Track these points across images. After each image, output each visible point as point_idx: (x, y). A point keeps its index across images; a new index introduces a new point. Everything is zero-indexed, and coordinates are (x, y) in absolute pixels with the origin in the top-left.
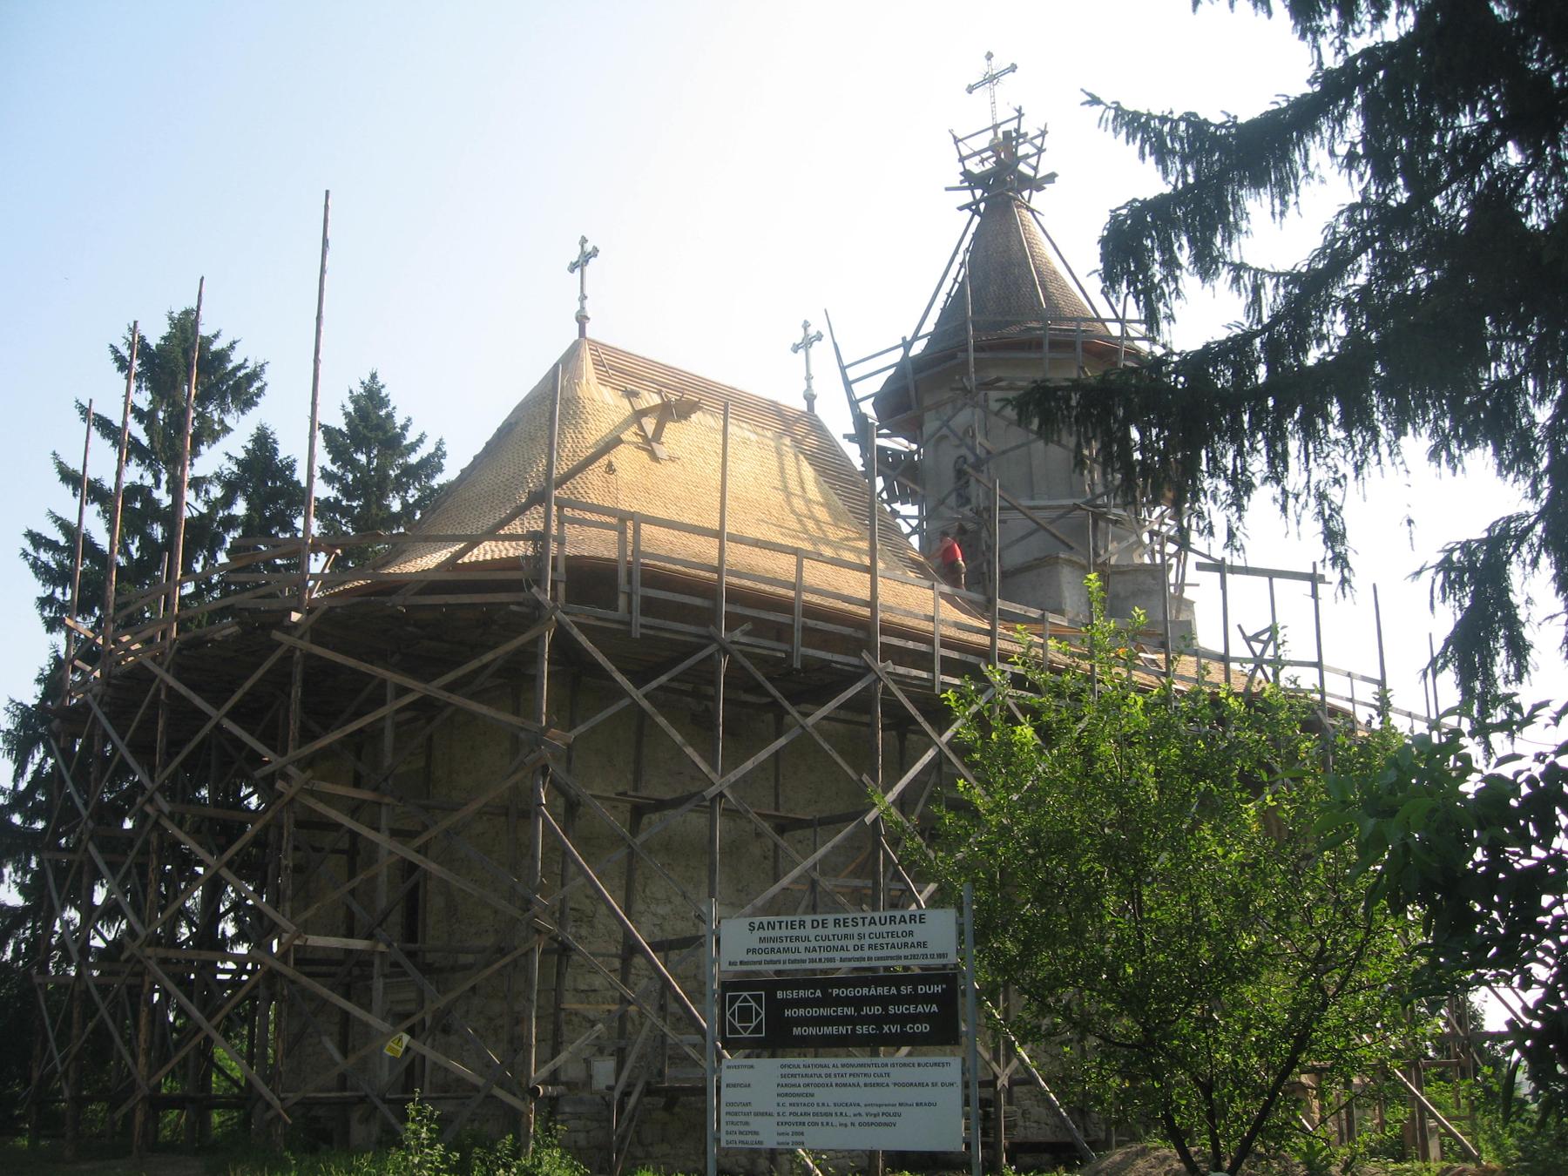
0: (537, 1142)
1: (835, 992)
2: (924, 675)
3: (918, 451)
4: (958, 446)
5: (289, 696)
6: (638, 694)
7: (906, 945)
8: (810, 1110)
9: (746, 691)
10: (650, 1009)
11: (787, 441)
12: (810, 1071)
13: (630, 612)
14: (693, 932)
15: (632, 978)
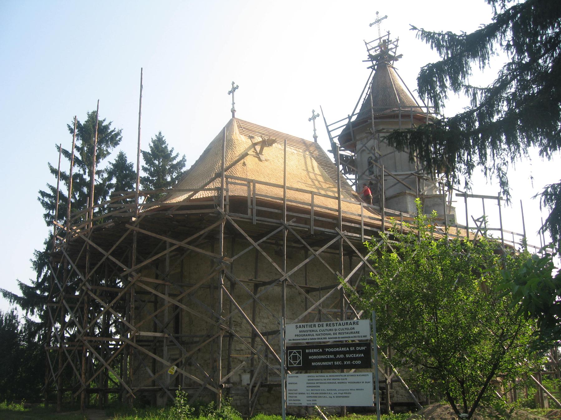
0: (223, 404)
1: (327, 350)
2: (358, 236)
3: (354, 156)
4: (369, 153)
6: (256, 244)
7: (352, 333)
10: (262, 356)
11: (307, 153)
13: (252, 215)
15: (255, 345)
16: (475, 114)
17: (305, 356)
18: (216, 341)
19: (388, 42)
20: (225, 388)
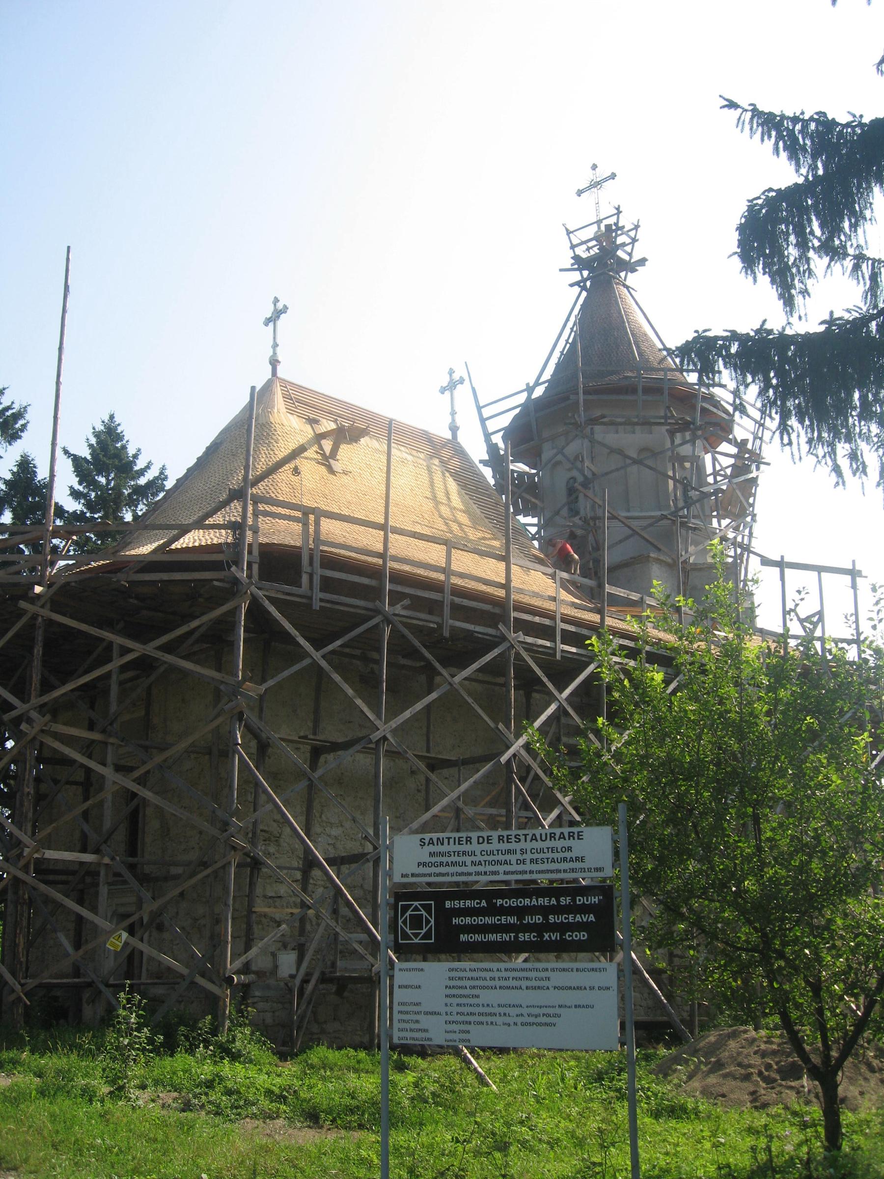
0: (232, 1022)
1: (499, 902)
2: (548, 644)
3: (537, 474)
4: (569, 470)
5: (32, 654)
6: (317, 655)
7: (565, 859)
8: (476, 1010)
10: (325, 912)
11: (436, 462)
13: (311, 588)
14: (361, 850)
15: (310, 887)
16: (873, 325)
17: (444, 916)
18: (220, 876)
19: (616, 231)
20: (238, 984)
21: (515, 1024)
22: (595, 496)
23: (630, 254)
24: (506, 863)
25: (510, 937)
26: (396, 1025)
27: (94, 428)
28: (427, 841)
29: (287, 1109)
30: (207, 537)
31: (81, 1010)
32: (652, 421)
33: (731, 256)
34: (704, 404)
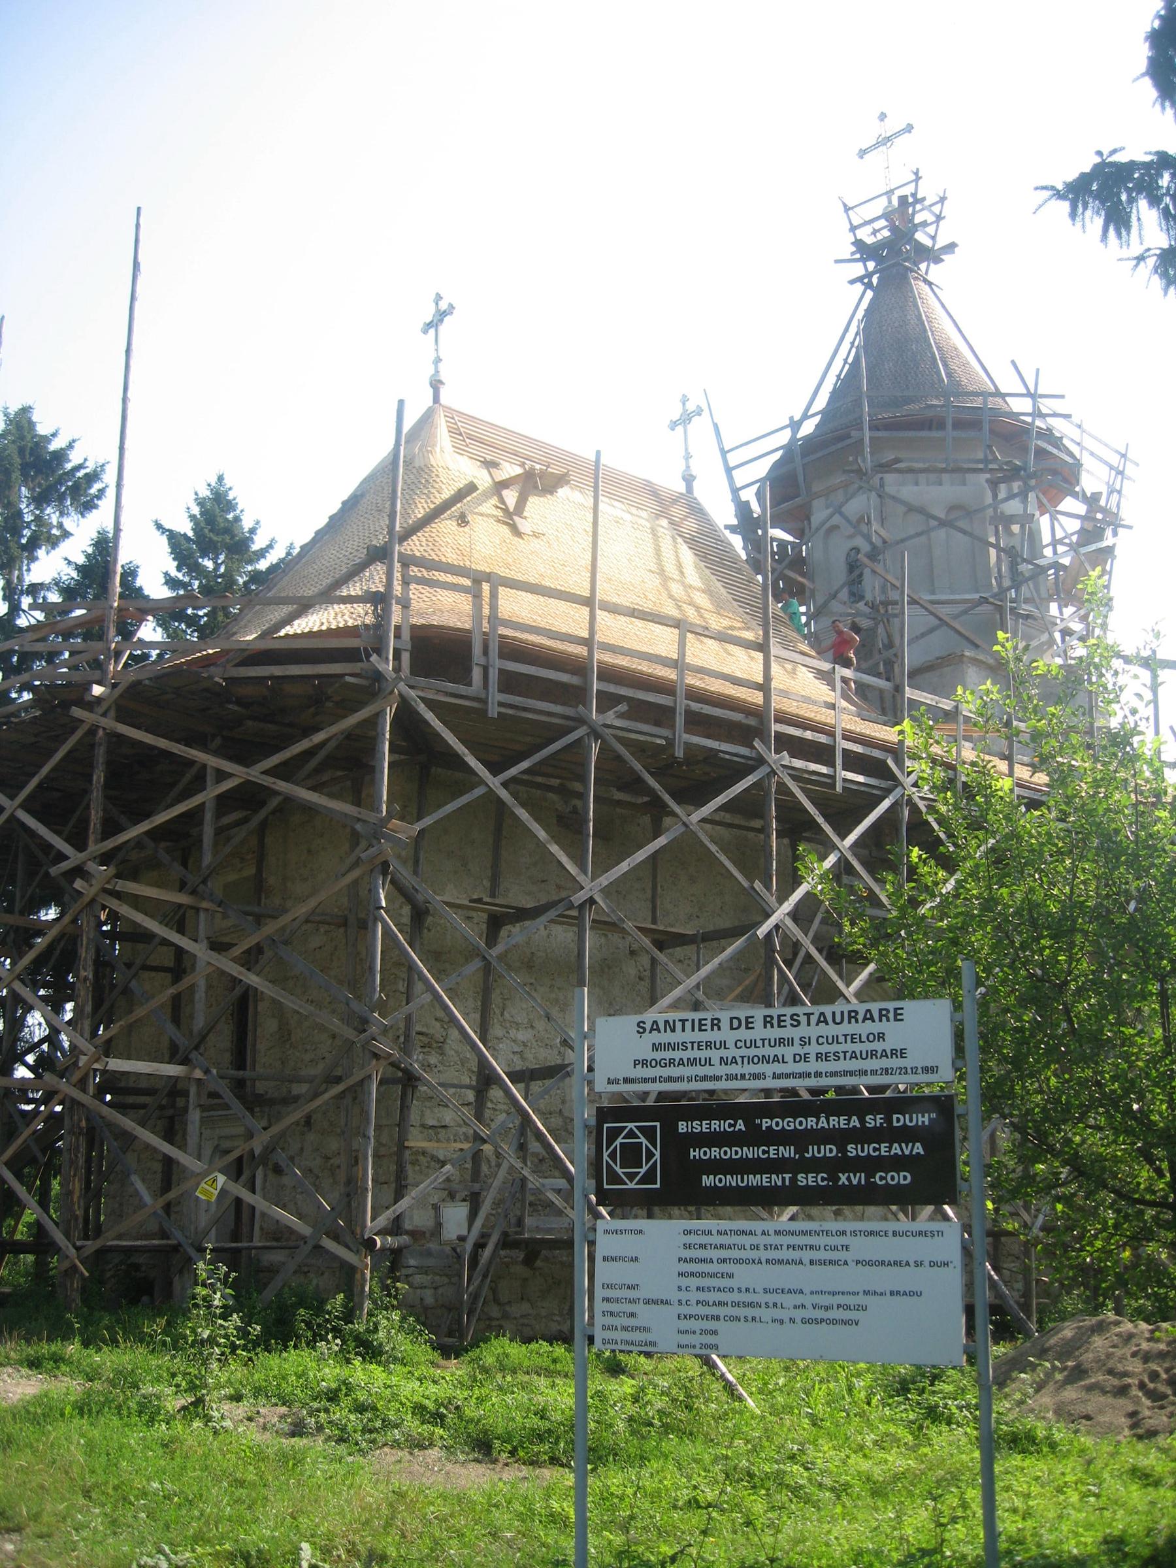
0: (374, 1302)
1: (766, 1123)
2: (824, 770)
4: (851, 537)
6: (494, 782)
7: (873, 1054)
9: (619, 789)
10: (508, 1149)
11: (664, 522)
12: (725, 1240)
14: (559, 1062)
15: (487, 1114)
17: (675, 1146)
19: (913, 204)
20: (383, 1249)
21: (792, 1320)
22: (887, 571)
23: (933, 238)
24: (776, 1059)
25: (784, 1179)
26: (599, 1320)
27: (196, 494)
28: (648, 1026)
29: (445, 1435)
30: (339, 619)
31: (171, 1284)
32: (965, 466)
33: (1138, 78)
34: (1039, 443)
